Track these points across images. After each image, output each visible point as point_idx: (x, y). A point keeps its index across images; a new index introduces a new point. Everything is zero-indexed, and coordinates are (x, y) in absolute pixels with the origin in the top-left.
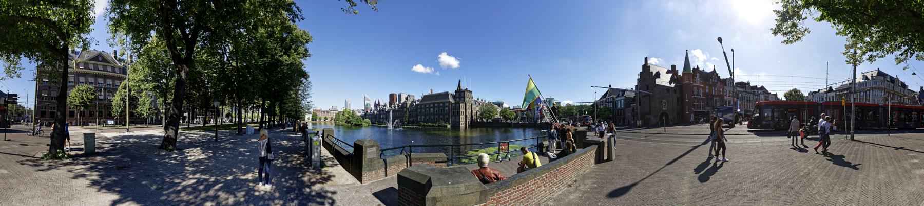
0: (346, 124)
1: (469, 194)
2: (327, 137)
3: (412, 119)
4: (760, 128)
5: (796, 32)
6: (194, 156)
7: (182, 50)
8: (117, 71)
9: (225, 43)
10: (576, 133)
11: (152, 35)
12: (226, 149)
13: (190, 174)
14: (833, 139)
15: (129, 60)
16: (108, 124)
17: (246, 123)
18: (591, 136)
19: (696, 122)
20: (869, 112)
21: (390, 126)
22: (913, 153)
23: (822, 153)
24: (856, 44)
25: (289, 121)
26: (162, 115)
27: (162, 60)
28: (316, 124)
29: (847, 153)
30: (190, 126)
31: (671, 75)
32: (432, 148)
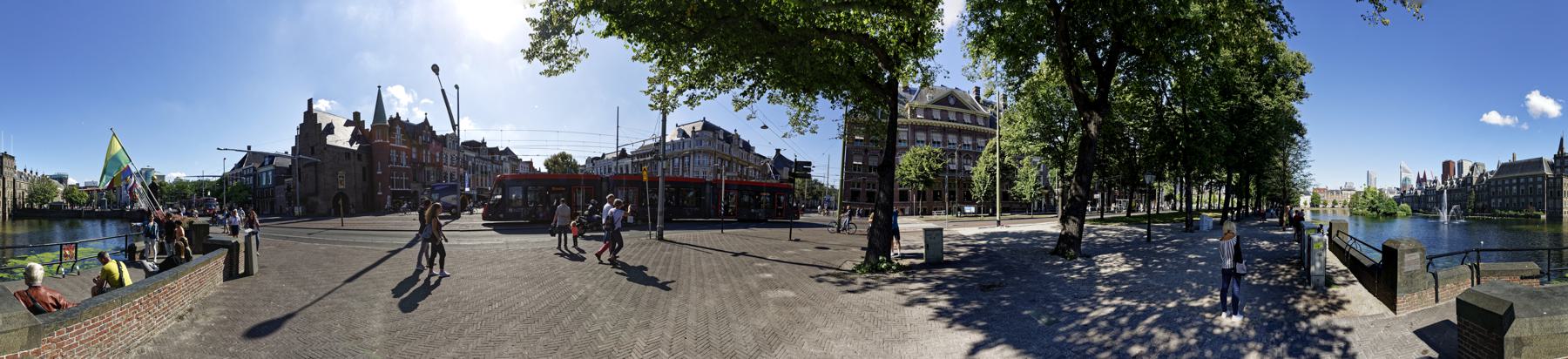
0: (1369, 213)
1: (9, 332)
2: (1337, 235)
3: (1480, 204)
4: (504, 219)
5: (564, 56)
6: (1111, 266)
7: (1090, 86)
8: (981, 122)
9: (1163, 75)
10: (192, 229)
11: (1040, 60)
12: (1166, 255)
13: (1105, 297)
14: (627, 238)
15: (1002, 103)
16: (965, 213)
17: (1199, 212)
18: (217, 233)
19: (395, 210)
20: (689, 191)
21: (1444, 216)
22: (763, 262)
23: (609, 262)
24: (667, 76)
25: (1272, 207)
26: (1057, 197)
27: (1057, 103)
28: (1318, 212)
29: (651, 262)
30: (1104, 217)
31: (352, 128)
32: (1515, 253)
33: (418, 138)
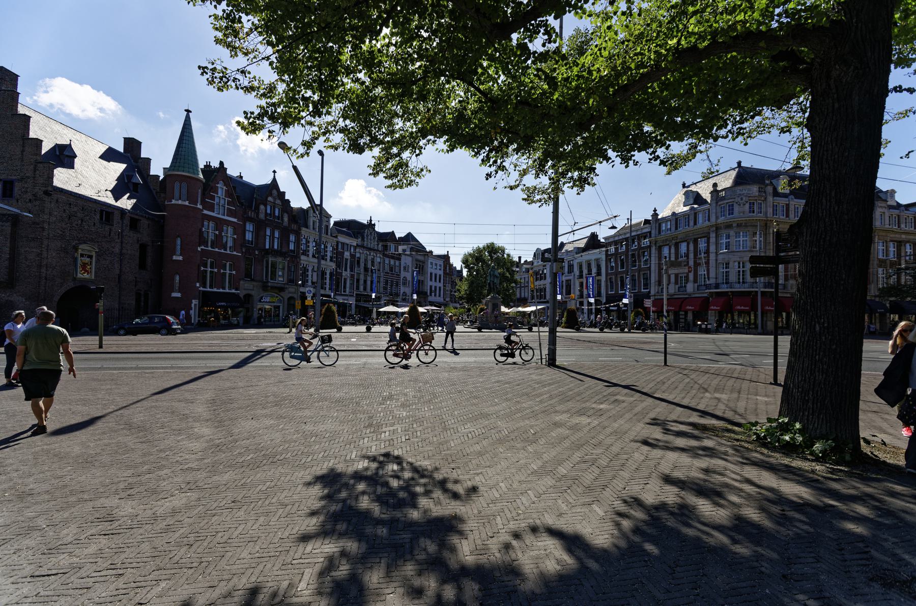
31: (120, 167)
33: (257, 208)
